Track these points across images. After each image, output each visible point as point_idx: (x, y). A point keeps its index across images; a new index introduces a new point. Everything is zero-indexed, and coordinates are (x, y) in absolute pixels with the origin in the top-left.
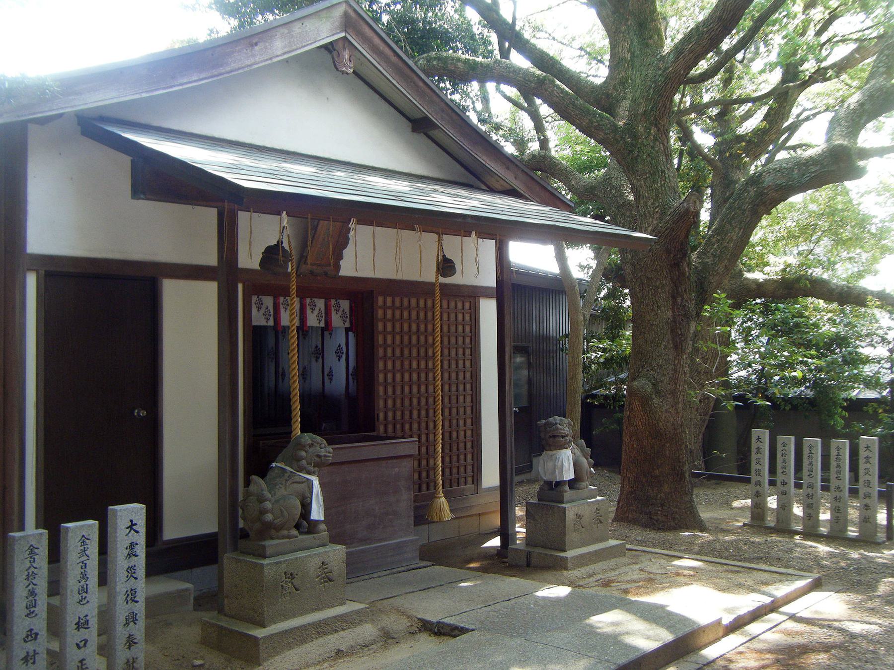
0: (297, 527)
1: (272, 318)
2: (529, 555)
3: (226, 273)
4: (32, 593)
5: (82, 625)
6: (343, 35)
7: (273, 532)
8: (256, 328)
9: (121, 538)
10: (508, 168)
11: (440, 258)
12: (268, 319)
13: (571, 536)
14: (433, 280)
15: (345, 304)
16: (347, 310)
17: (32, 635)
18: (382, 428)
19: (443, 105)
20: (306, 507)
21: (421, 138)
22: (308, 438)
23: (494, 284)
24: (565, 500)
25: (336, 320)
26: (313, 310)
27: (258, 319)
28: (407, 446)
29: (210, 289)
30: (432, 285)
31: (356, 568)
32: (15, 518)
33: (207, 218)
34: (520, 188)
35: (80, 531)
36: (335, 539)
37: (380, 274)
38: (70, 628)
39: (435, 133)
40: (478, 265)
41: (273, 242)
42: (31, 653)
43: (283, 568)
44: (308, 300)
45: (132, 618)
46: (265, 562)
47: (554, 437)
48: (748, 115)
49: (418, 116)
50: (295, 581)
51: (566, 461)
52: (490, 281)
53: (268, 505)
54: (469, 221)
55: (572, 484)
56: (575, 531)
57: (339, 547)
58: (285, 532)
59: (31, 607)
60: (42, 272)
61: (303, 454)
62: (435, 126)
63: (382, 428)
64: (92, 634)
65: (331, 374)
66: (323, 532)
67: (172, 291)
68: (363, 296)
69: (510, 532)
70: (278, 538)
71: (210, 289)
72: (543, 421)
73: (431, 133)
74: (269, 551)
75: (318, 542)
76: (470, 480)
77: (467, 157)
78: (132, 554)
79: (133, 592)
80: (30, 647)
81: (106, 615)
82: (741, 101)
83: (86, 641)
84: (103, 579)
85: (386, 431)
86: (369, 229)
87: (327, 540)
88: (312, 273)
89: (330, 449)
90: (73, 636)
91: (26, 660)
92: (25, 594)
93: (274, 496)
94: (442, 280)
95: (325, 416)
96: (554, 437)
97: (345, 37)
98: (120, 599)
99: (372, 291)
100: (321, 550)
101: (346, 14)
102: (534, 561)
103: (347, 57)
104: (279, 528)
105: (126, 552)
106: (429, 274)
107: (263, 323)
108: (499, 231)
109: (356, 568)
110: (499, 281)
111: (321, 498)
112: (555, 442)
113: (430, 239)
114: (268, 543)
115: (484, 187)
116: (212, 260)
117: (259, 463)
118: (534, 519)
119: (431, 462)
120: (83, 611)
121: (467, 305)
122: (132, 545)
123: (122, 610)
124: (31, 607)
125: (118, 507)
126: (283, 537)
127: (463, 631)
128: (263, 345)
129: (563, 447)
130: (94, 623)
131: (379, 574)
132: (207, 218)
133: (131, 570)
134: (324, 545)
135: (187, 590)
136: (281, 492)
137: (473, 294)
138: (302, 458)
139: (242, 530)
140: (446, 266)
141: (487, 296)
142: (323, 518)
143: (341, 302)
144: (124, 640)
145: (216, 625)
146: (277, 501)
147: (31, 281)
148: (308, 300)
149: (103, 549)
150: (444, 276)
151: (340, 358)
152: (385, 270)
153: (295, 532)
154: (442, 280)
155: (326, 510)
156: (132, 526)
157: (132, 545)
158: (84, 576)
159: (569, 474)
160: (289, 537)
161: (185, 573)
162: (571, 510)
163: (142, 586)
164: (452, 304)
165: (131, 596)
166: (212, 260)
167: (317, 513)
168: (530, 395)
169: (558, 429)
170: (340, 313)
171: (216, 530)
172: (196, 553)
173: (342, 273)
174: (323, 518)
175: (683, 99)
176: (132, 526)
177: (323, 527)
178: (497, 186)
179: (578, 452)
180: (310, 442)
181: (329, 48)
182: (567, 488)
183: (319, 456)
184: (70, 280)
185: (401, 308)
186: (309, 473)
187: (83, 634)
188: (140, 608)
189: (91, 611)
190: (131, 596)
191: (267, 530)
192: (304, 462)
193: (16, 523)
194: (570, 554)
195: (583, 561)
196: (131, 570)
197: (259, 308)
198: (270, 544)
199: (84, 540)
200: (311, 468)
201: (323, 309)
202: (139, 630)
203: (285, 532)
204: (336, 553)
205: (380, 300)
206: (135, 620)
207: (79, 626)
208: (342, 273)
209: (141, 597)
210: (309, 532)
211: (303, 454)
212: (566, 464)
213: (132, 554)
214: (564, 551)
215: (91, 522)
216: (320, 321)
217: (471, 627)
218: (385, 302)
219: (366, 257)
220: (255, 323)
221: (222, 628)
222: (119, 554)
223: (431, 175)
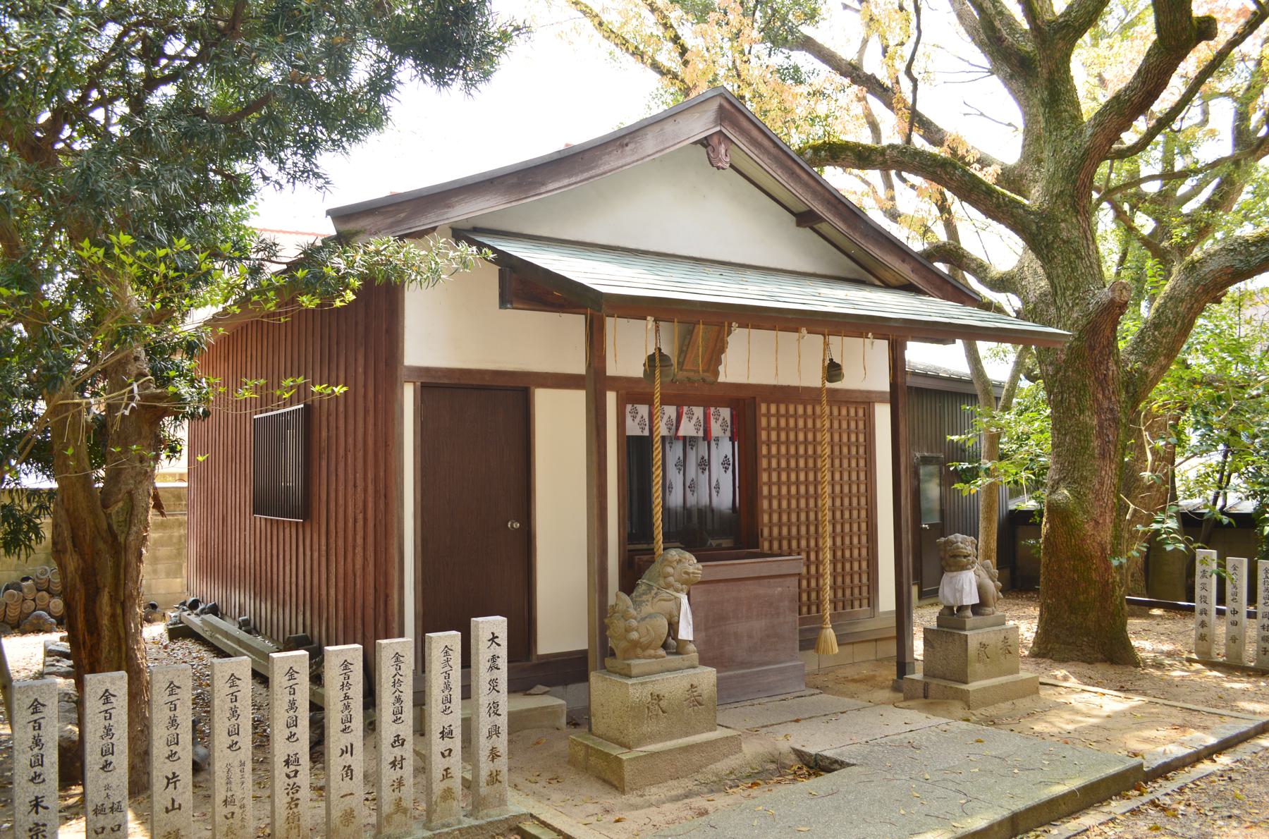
0: (665, 646)
1: (647, 428)
2: (926, 686)
3: (594, 382)
4: (399, 700)
5: (446, 734)
6: (718, 129)
7: (639, 651)
8: (632, 439)
9: (483, 652)
10: (903, 261)
11: (827, 362)
12: (643, 429)
13: (975, 667)
14: (819, 385)
15: (726, 413)
16: (728, 419)
17: (399, 741)
18: (766, 545)
19: (827, 195)
20: (673, 627)
21: (806, 232)
22: (674, 554)
23: (887, 388)
24: (968, 626)
25: (716, 429)
26: (690, 419)
27: (633, 429)
28: (793, 564)
29: (577, 399)
30: (817, 391)
31: (728, 694)
32: (396, 625)
33: (575, 325)
34: (915, 279)
35: (446, 641)
36: (704, 661)
37: (755, 379)
38: (436, 736)
39: (823, 227)
40: (867, 369)
41: (651, 351)
42: (399, 758)
43: (650, 688)
44: (685, 408)
45: (495, 731)
46: (630, 682)
47: (955, 556)
48: (1196, 191)
49: (802, 208)
50: (661, 703)
51: (967, 585)
52: (884, 385)
53: (634, 623)
54: (892, 324)
55: (976, 609)
56: (979, 661)
57: (710, 669)
58: (652, 652)
59: (398, 713)
60: (418, 384)
61: (670, 570)
62: (821, 219)
63: (766, 545)
64: (456, 744)
65: (718, 487)
66: (693, 652)
67: (543, 399)
68: (745, 406)
69: (908, 660)
70: (644, 658)
71: (577, 399)
72: (943, 539)
73: (816, 227)
74: (634, 671)
75: (687, 663)
76: (865, 602)
77: (862, 251)
78: (494, 667)
79: (496, 704)
80: (398, 752)
81: (468, 726)
82: (1184, 175)
83: (450, 750)
84: (467, 693)
85: (780, 547)
86: (746, 330)
87: (696, 662)
88: (689, 379)
89: (700, 566)
90: (438, 745)
91: (393, 764)
92: (392, 700)
93: (642, 615)
94: (828, 385)
95: (695, 531)
96: (955, 556)
97: (720, 131)
98: (483, 711)
99: (754, 398)
100: (692, 671)
101: (721, 106)
102: (931, 693)
103: (723, 151)
104: (645, 647)
105: (488, 665)
106: (813, 378)
107: (637, 432)
108: (897, 333)
109: (728, 694)
110: (893, 385)
111: (690, 616)
112: (955, 562)
113: (814, 342)
114: (633, 662)
115: (878, 283)
116: (578, 366)
117: (631, 577)
118: (932, 647)
119: (821, 582)
120: (446, 720)
121: (861, 413)
122: (494, 658)
123: (484, 723)
124: (398, 713)
125: (480, 619)
126: (650, 657)
127: (843, 765)
128: (638, 453)
129: (963, 568)
130: (457, 732)
131: (761, 701)
132: (575, 325)
133: (493, 683)
134: (694, 667)
135: (560, 706)
136: (647, 609)
137: (865, 401)
138: (669, 575)
139: (605, 650)
140: (833, 371)
141: (882, 402)
142: (691, 638)
143: (694, 409)
144: (487, 753)
145: (581, 743)
146: (643, 619)
147: (408, 393)
148: (685, 408)
149: (466, 663)
150: (830, 381)
151: (726, 469)
152: (761, 374)
153: (662, 652)
154: (828, 385)
155: (696, 629)
156: (494, 638)
157: (494, 658)
158: (448, 686)
159: (971, 598)
160: (656, 657)
161: (559, 689)
162: (974, 638)
163: (503, 697)
164: (844, 412)
165: (494, 709)
166: (578, 366)
167: (686, 632)
168: (942, 512)
169: (958, 548)
170: (720, 422)
171: (585, 647)
172: (570, 670)
173: (721, 379)
174: (691, 638)
175: (1108, 172)
176: (494, 638)
177: (692, 647)
178: (893, 281)
179: (984, 574)
180: (677, 557)
181: (705, 142)
182: (969, 613)
183: (686, 573)
184: (442, 389)
185: (787, 416)
186: (677, 591)
187: (448, 743)
188: (503, 722)
189: (455, 721)
190: (494, 709)
191: (636, 648)
192: (671, 579)
193: (396, 631)
194: (972, 686)
195: (989, 698)
196: (493, 683)
197: (634, 418)
198: (637, 664)
199: (447, 650)
200: (679, 585)
201: (701, 418)
202: (502, 743)
203: (652, 652)
204: (707, 677)
205: (764, 408)
206: (498, 734)
207: (443, 735)
208: (721, 379)
209: (504, 709)
210: (677, 653)
211: (670, 570)
212: (966, 587)
213: (494, 667)
214: (966, 683)
215: (454, 632)
216: (698, 430)
217: (852, 761)
218: (768, 409)
219: (746, 362)
220: (629, 432)
221: (587, 746)
222: (481, 666)
223: (818, 272)
